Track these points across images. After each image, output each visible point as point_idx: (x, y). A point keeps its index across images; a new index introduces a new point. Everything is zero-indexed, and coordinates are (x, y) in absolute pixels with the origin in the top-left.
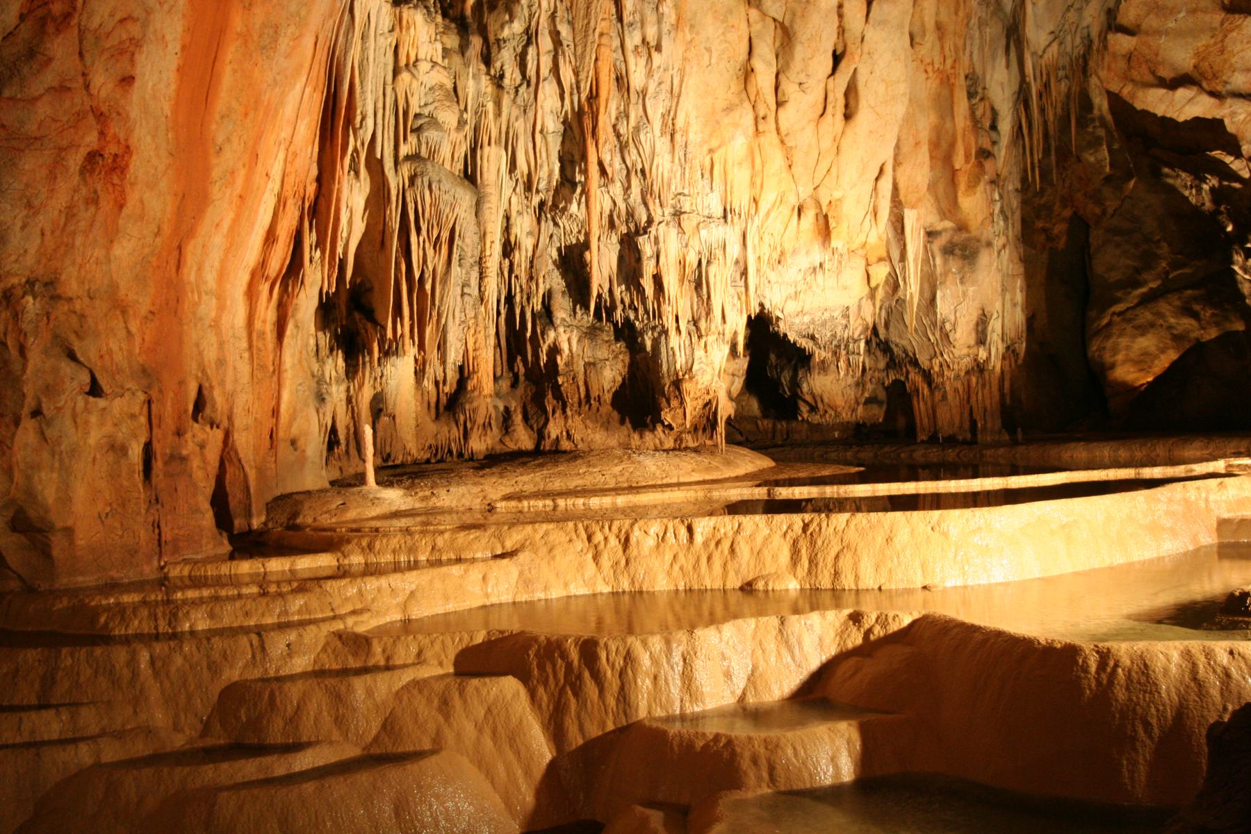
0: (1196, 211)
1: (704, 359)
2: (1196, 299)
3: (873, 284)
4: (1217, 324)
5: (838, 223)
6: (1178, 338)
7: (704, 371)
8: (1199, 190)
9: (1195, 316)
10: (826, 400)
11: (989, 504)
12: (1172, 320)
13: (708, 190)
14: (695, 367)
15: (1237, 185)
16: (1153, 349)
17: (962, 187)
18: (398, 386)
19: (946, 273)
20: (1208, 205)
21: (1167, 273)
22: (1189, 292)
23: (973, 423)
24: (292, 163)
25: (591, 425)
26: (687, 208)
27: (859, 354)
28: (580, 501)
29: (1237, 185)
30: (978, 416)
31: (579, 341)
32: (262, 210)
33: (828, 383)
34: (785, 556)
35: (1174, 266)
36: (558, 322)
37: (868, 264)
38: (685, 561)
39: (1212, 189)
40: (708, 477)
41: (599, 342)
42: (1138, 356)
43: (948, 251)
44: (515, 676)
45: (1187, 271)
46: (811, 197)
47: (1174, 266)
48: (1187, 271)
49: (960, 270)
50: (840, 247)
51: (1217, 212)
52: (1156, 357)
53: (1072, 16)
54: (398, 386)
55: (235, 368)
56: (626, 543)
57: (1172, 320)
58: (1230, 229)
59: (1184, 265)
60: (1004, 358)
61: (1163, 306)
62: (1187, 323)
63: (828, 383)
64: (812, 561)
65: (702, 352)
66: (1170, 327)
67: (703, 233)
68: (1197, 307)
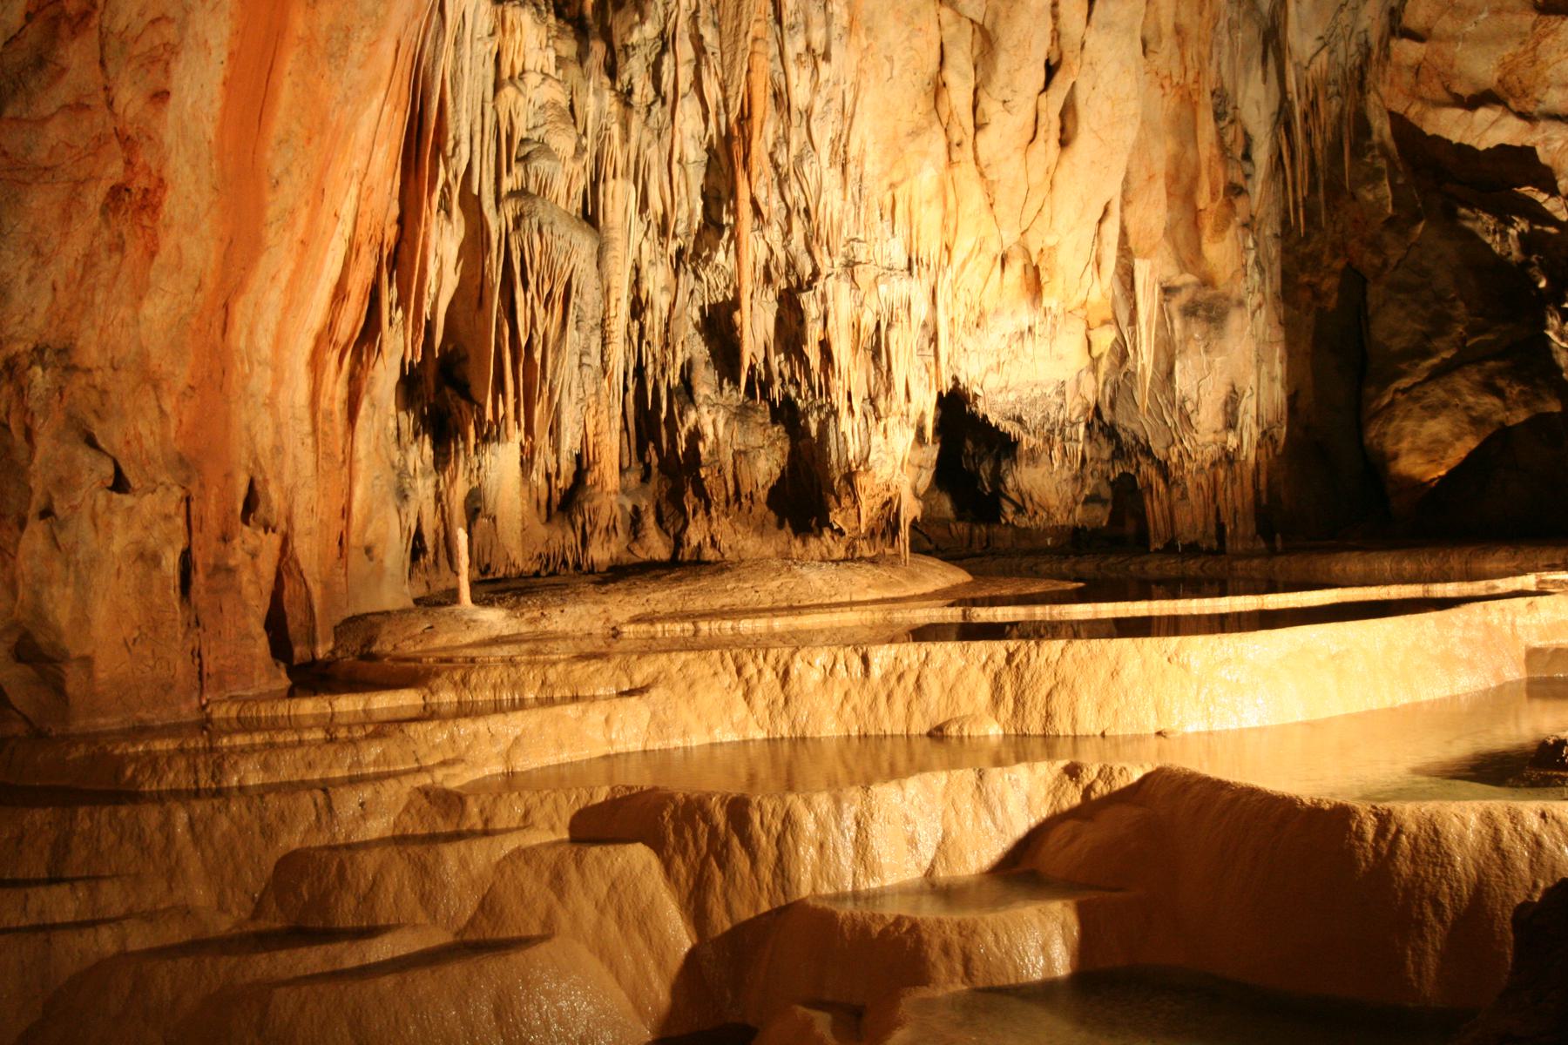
0: (1501, 262)
2: (1501, 373)
3: (1095, 353)
4: (1526, 404)
5: (1051, 276)
6: (1477, 422)
7: (884, 462)
8: (1505, 235)
9: (1499, 393)
10: (1036, 498)
11: (1240, 629)
12: (1471, 399)
13: (889, 234)
14: (872, 457)
15: (1552, 230)
16: (1445, 435)
17: (1207, 232)
18: (500, 479)
19: (1186, 340)
20: (1516, 255)
21: (1464, 340)
22: (1492, 364)
23: (1221, 527)
25: (741, 529)
26: (862, 257)
27: (1077, 441)
29: (1552, 230)
30: (1226, 518)
31: (726, 423)
33: (1039, 476)
34: (984, 693)
35: (1473, 330)
37: (1089, 328)
38: (859, 699)
39: (1521, 235)
42: (1426, 444)
43: (1189, 311)
45: (1489, 337)
46: (1018, 243)
47: (1473, 330)
48: (1489, 337)
49: (1205, 336)
51: (1526, 264)
52: (1451, 445)
53: (1345, 17)
54: (500, 479)
55: (295, 457)
56: (785, 677)
57: (1471, 399)
58: (1542, 284)
59: (1484, 330)
61: (1460, 382)
62: (1488, 402)
63: (1039, 476)
64: (1019, 700)
65: (881, 438)
66: (1468, 408)
67: (883, 288)
68: (1501, 383)
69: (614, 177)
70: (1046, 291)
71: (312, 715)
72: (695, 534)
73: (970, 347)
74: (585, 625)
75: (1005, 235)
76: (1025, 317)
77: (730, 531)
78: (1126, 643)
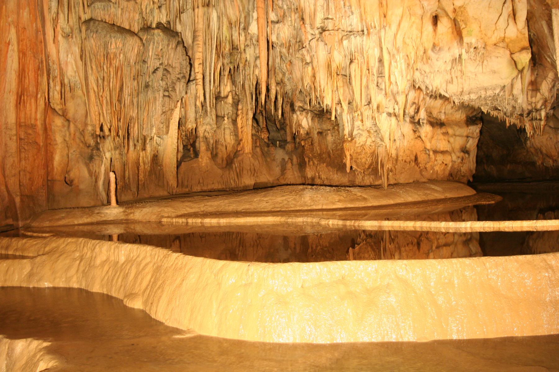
1: (361, 127)
3: (520, 67)
5: (466, 24)
7: (361, 135)
10: (544, 152)
11: (232, 255)
13: (349, 13)
14: (355, 133)
18: (164, 150)
24: (37, 31)
25: (331, 170)
26: (330, 27)
27: (540, 120)
28: (199, 220)
31: (312, 119)
32: (9, 61)
33: (544, 140)
36: (296, 108)
37: (512, 54)
40: (349, 205)
41: (324, 119)
44: (151, 318)
46: (439, 7)
50: (473, 41)
54: (164, 150)
55: (6, 144)
60: (477, 124)
63: (544, 140)
65: (360, 123)
67: (345, 43)
69: (198, 7)
70: (464, 33)
71: (444, 228)
72: (310, 173)
73: (428, 70)
74: (147, 218)
75: (425, 4)
76: (456, 51)
77: (327, 170)
78: (176, 259)
